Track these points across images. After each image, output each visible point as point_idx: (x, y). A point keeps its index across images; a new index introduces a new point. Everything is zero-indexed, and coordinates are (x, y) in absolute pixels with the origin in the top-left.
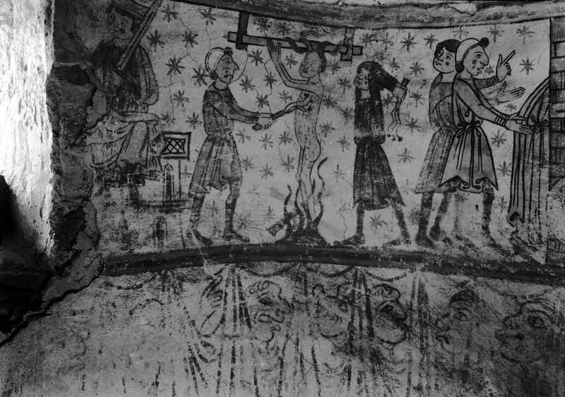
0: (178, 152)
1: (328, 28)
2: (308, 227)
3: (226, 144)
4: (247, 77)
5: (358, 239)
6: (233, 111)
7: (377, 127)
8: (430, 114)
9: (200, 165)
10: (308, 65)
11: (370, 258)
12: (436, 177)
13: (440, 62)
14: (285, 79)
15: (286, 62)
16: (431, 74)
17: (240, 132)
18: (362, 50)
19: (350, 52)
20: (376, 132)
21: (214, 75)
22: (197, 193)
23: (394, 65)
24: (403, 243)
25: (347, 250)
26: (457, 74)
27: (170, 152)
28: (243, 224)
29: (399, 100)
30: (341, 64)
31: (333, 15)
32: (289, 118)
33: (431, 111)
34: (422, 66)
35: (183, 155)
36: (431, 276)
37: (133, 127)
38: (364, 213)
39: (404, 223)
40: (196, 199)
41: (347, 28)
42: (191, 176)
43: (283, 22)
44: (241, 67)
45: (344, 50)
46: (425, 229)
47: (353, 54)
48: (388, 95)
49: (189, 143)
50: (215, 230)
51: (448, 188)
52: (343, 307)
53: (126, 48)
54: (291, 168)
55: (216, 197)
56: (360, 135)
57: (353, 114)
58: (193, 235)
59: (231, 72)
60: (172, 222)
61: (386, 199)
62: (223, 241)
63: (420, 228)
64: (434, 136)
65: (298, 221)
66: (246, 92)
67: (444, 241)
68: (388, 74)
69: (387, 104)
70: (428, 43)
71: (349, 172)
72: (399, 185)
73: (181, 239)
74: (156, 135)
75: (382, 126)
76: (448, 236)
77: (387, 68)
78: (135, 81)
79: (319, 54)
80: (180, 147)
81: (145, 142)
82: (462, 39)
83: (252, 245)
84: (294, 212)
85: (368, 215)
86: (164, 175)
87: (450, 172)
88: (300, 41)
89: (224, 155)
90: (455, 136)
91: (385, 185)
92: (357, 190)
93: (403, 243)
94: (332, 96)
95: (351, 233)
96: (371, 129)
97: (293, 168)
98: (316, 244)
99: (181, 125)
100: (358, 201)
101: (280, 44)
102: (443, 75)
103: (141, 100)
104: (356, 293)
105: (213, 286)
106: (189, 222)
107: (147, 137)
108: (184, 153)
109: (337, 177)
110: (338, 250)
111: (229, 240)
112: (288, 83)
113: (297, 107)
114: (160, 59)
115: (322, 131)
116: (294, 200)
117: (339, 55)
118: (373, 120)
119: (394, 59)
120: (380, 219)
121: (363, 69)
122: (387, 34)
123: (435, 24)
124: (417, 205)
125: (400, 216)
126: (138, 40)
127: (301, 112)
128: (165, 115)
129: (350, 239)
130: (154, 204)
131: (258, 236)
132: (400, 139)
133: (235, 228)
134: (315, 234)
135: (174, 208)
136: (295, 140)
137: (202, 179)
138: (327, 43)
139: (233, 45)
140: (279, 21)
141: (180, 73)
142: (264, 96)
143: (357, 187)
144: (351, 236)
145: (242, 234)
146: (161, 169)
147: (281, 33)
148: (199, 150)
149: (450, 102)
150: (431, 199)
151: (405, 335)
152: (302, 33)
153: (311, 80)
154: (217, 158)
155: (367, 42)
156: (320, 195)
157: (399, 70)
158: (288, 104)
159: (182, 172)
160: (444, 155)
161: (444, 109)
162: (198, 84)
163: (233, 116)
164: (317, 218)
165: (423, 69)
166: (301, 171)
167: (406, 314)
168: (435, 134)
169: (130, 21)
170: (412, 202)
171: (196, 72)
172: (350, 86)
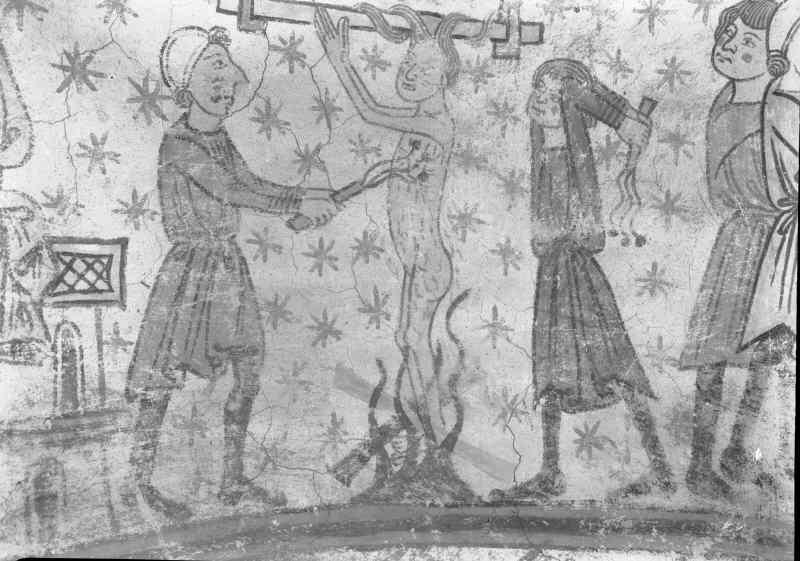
0: (93, 289)
2: (429, 459)
3: (221, 265)
4: (268, 102)
5: (548, 483)
7: (584, 215)
13: (729, 54)
14: (362, 107)
15: (364, 64)
17: (257, 235)
18: (542, 32)
19: (514, 37)
20: (583, 225)
22: (147, 389)
23: (619, 66)
24: (656, 489)
26: (773, 81)
27: (72, 289)
28: (268, 459)
29: (635, 149)
30: (495, 67)
32: (375, 198)
33: (713, 173)
35: (109, 296)
38: (560, 419)
39: (655, 440)
40: (145, 403)
42: (131, 348)
46: (708, 453)
48: (608, 138)
49: (123, 264)
50: (198, 478)
51: (761, 354)
56: (547, 234)
57: (526, 184)
58: (140, 498)
62: (221, 505)
63: (696, 457)
64: (721, 232)
65: (404, 445)
66: (269, 137)
67: (758, 483)
68: (605, 87)
69: (608, 160)
71: (521, 321)
72: (641, 351)
73: (105, 511)
74: (28, 246)
75: (597, 209)
77: (601, 73)
79: (441, 44)
80: (100, 276)
83: (294, 511)
84: (394, 424)
85: (569, 424)
86: (54, 348)
89: (216, 293)
94: (476, 143)
95: (531, 468)
97: (388, 317)
98: (448, 499)
99: (98, 219)
100: (543, 393)
102: (737, 83)
106: (128, 467)
109: (494, 336)
111: (234, 504)
112: (369, 115)
113: (391, 174)
115: (455, 229)
116: (394, 395)
117: (490, 44)
118: (574, 197)
119: (619, 52)
120: (597, 434)
124: (688, 397)
125: (645, 422)
128: (55, 195)
129: (529, 483)
130: (27, 427)
132: (641, 241)
133: (249, 471)
135: (86, 433)
136: (390, 250)
137: (163, 353)
141: (94, 89)
142: (312, 148)
143: (542, 359)
144: (532, 475)
145: (269, 487)
146: (47, 333)
148: (151, 281)
149: (758, 149)
150: (718, 380)
153: (425, 106)
155: (553, 13)
156: (454, 381)
157: (631, 77)
158: (370, 164)
159: (105, 337)
160: (746, 276)
162: (142, 116)
163: (237, 197)
165: (689, 73)
168: (724, 226)
170: (673, 386)
171: (137, 86)
172: (516, 119)
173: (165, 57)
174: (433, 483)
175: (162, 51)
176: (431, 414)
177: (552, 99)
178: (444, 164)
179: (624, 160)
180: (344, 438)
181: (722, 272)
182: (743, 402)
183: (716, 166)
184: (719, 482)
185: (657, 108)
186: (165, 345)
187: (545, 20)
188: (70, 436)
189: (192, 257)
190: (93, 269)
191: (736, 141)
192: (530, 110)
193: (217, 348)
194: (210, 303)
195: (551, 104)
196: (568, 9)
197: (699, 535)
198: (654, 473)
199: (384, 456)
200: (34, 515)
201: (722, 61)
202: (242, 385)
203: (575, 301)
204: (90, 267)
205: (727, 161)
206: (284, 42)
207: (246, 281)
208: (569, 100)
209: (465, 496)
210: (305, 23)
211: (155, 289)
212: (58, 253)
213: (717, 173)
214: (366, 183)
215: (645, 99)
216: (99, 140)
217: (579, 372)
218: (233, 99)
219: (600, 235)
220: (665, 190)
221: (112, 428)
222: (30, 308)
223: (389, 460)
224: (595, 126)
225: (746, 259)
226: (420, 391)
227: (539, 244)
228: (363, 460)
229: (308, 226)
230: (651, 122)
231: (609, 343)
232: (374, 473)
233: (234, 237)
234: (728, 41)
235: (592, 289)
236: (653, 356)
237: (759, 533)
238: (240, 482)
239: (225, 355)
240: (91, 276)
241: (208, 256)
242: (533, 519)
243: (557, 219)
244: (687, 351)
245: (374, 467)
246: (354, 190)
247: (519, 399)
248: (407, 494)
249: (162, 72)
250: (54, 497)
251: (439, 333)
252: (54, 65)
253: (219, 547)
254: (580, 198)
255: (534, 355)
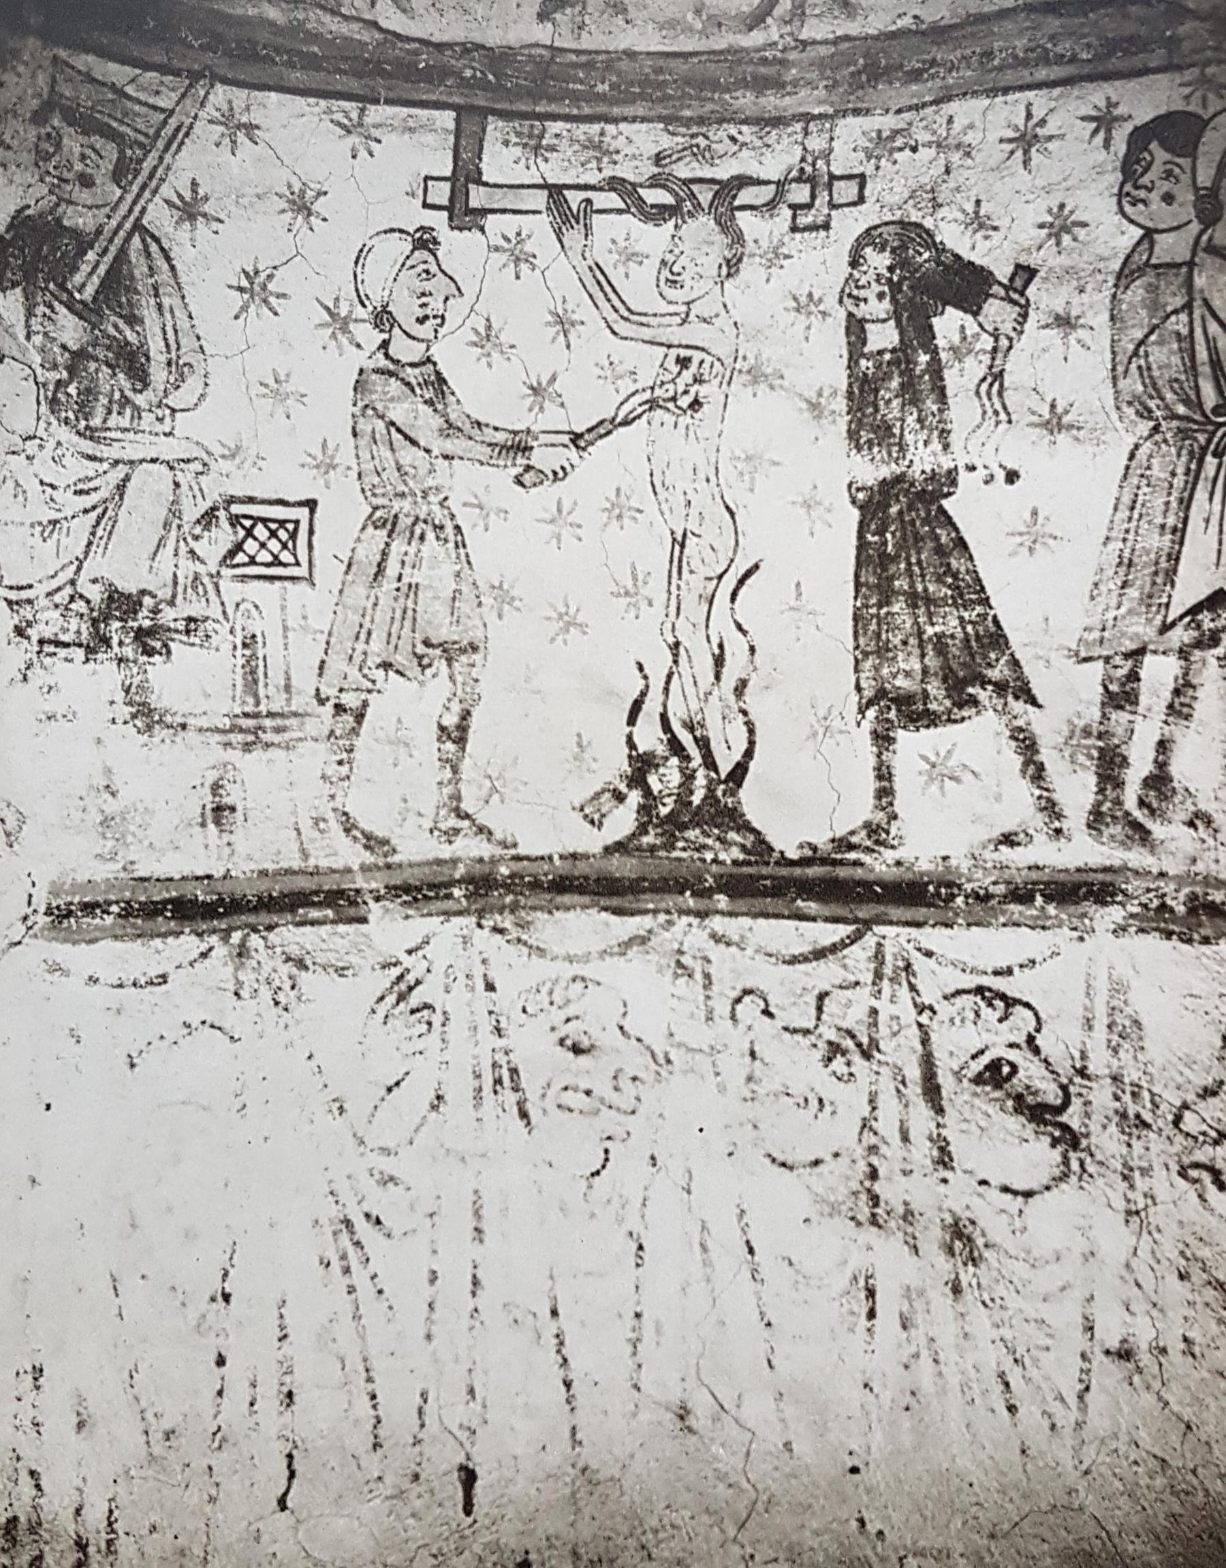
0: (277, 562)
1: (744, 128)
3: (430, 535)
6: (450, 428)
7: (926, 443)
8: (1115, 379)
9: (350, 602)
10: (683, 261)
11: (921, 896)
12: (1147, 599)
13: (1142, 194)
14: (612, 316)
16: (1114, 237)
18: (862, 187)
19: (822, 198)
20: (923, 458)
21: (383, 318)
22: (341, 690)
23: (979, 222)
24: (1040, 838)
25: (842, 872)
27: (252, 561)
29: (1004, 342)
31: (761, 85)
33: (1120, 369)
34: (1079, 216)
36: (1153, 948)
37: (127, 478)
39: (1041, 767)
40: (339, 708)
41: (807, 118)
43: (596, 128)
44: (469, 290)
45: (800, 193)
46: (1119, 785)
47: (833, 206)
49: (311, 532)
51: (1196, 634)
52: (838, 1064)
53: (99, 232)
54: (643, 605)
55: (409, 707)
56: (871, 470)
57: (841, 404)
59: (436, 305)
60: (257, 777)
61: (971, 690)
64: (1132, 456)
65: (675, 778)
67: (1191, 824)
68: (957, 257)
70: (1096, 132)
74: (204, 506)
76: (1203, 806)
77: (954, 237)
78: (131, 337)
81: (166, 525)
82: (1211, 111)
85: (911, 744)
87: (1192, 586)
88: (655, 182)
90: (1204, 450)
91: (967, 639)
92: (868, 664)
93: (1040, 838)
95: (860, 808)
96: (902, 448)
98: (736, 853)
101: (589, 201)
103: (149, 394)
104: (882, 1018)
105: (403, 988)
107: (175, 512)
108: (298, 564)
110: (813, 871)
113: (653, 404)
114: (205, 265)
117: (788, 213)
121: (868, 251)
122: (950, 120)
123: (1115, 63)
125: (1027, 744)
126: (138, 208)
127: (669, 419)
129: (852, 833)
130: (204, 722)
131: (550, 827)
132: (1012, 477)
134: (733, 818)
135: (268, 737)
138: (744, 181)
139: (438, 220)
140: (584, 127)
143: (866, 654)
147: (594, 164)
149: (1185, 331)
150: (1134, 676)
151: (1066, 1161)
152: (658, 159)
153: (696, 309)
154: (405, 580)
155: (878, 158)
157: (997, 236)
160: (1171, 521)
161: (1164, 356)
164: (738, 764)
165: (1084, 225)
166: (678, 614)
167: (1064, 1088)
168: (1137, 447)
169: (111, 152)
170: (1068, 694)
171: (327, 309)
173: (359, 270)
174: (716, 831)
175: (356, 263)
176: (711, 735)
177: (878, 281)
178: (724, 386)
179: (986, 359)
180: (594, 766)
181: (1136, 516)
182: (1171, 706)
183: (1126, 361)
184: (1137, 826)
185: (1036, 280)
186: (363, 637)
187: (869, 169)
188: (251, 738)
189: (394, 524)
190: (277, 537)
191: (1155, 321)
192: (845, 299)
193: (427, 643)
194: (417, 585)
195: (876, 288)
196: (901, 149)
197: (1104, 903)
198: (1040, 815)
199: (647, 792)
200: (211, 826)
201: (1134, 205)
202: (459, 693)
203: (916, 569)
204: (273, 534)
205: (1142, 352)
206: (508, 240)
207: (463, 558)
208: (902, 279)
209: (761, 847)
210: (534, 212)
211: (350, 565)
212: (237, 516)
213: (1126, 371)
214: (618, 420)
215: (1018, 266)
216: (282, 378)
217: (925, 671)
218: (443, 317)
219: (949, 472)
220: (1049, 400)
221: (300, 735)
222: (206, 580)
223: (655, 799)
224: (942, 313)
225: (1169, 494)
226: (694, 705)
227: (858, 490)
228: (620, 797)
229: (541, 483)
230: (1028, 300)
231: (969, 628)
232: (635, 815)
233: (446, 499)
234: (1142, 175)
235: (940, 551)
236: (1035, 645)
237: (1193, 897)
238: (459, 816)
239: (438, 652)
240: (274, 545)
241: (414, 524)
242: (860, 883)
243: (884, 453)
244: (1086, 635)
245: (635, 807)
246: (603, 429)
247: (835, 712)
248: (680, 844)
249: (357, 290)
250: (233, 809)
251: (721, 625)
252: (230, 287)
253: (431, 894)
254: (920, 420)
255: (857, 648)
